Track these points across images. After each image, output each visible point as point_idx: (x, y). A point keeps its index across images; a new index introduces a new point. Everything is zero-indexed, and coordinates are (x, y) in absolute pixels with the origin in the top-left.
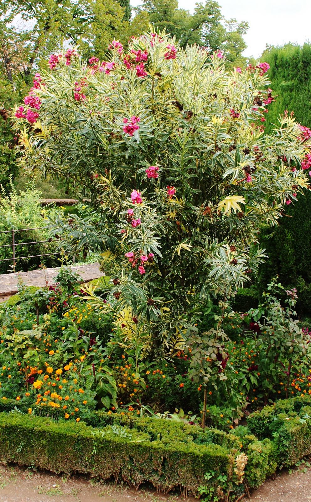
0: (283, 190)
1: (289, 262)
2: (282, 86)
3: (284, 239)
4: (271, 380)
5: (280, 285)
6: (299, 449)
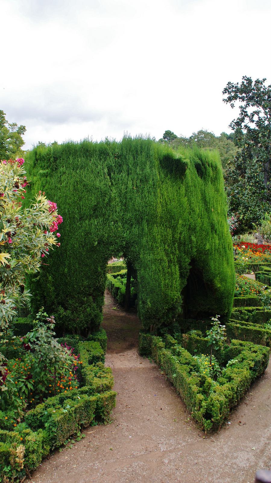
0: (39, 247)
1: (52, 296)
2: (40, 173)
3: (47, 281)
4: (44, 384)
5: (45, 314)
6: (64, 432)
